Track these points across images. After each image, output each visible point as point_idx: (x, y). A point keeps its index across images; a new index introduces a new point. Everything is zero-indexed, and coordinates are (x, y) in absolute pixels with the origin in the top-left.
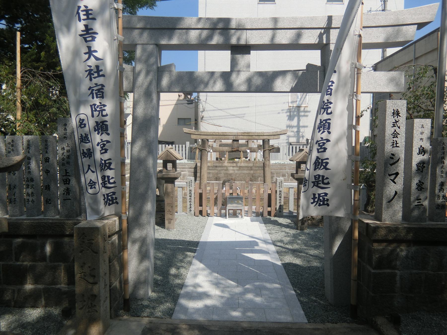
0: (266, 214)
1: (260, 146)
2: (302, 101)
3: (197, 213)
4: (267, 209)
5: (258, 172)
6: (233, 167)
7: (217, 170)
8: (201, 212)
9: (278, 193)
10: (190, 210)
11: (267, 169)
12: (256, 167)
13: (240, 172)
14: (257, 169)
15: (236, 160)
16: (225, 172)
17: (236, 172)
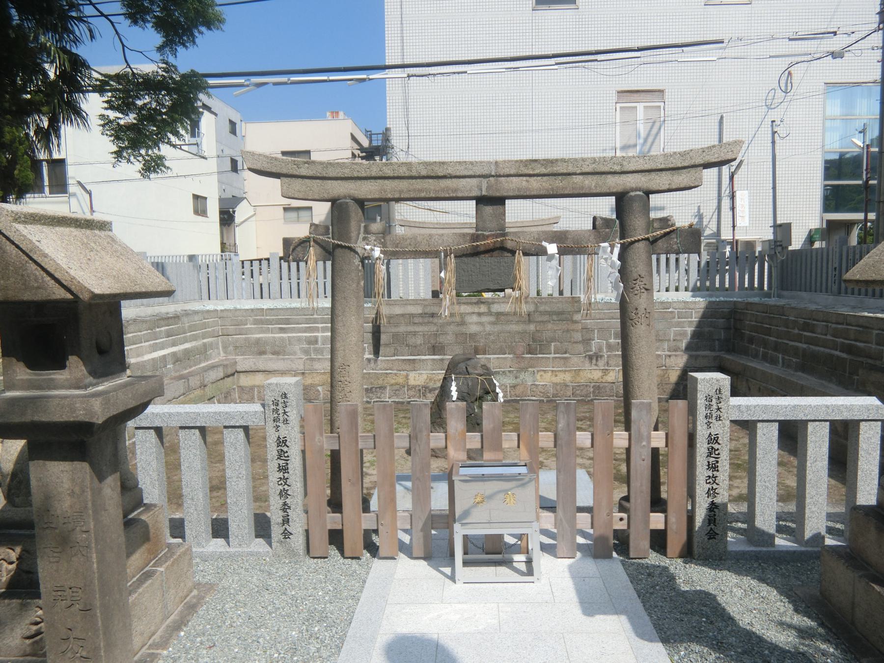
0: (640, 543)
1: (607, 222)
2: (649, 143)
3: (320, 539)
4: (647, 521)
5: (550, 326)
6: (480, 314)
7: (435, 324)
8: (336, 538)
9: (702, 448)
10: (287, 534)
11: (640, 331)
12: (543, 313)
13: (497, 328)
14: (546, 318)
15: (486, 295)
16: (457, 329)
17: (488, 328)
